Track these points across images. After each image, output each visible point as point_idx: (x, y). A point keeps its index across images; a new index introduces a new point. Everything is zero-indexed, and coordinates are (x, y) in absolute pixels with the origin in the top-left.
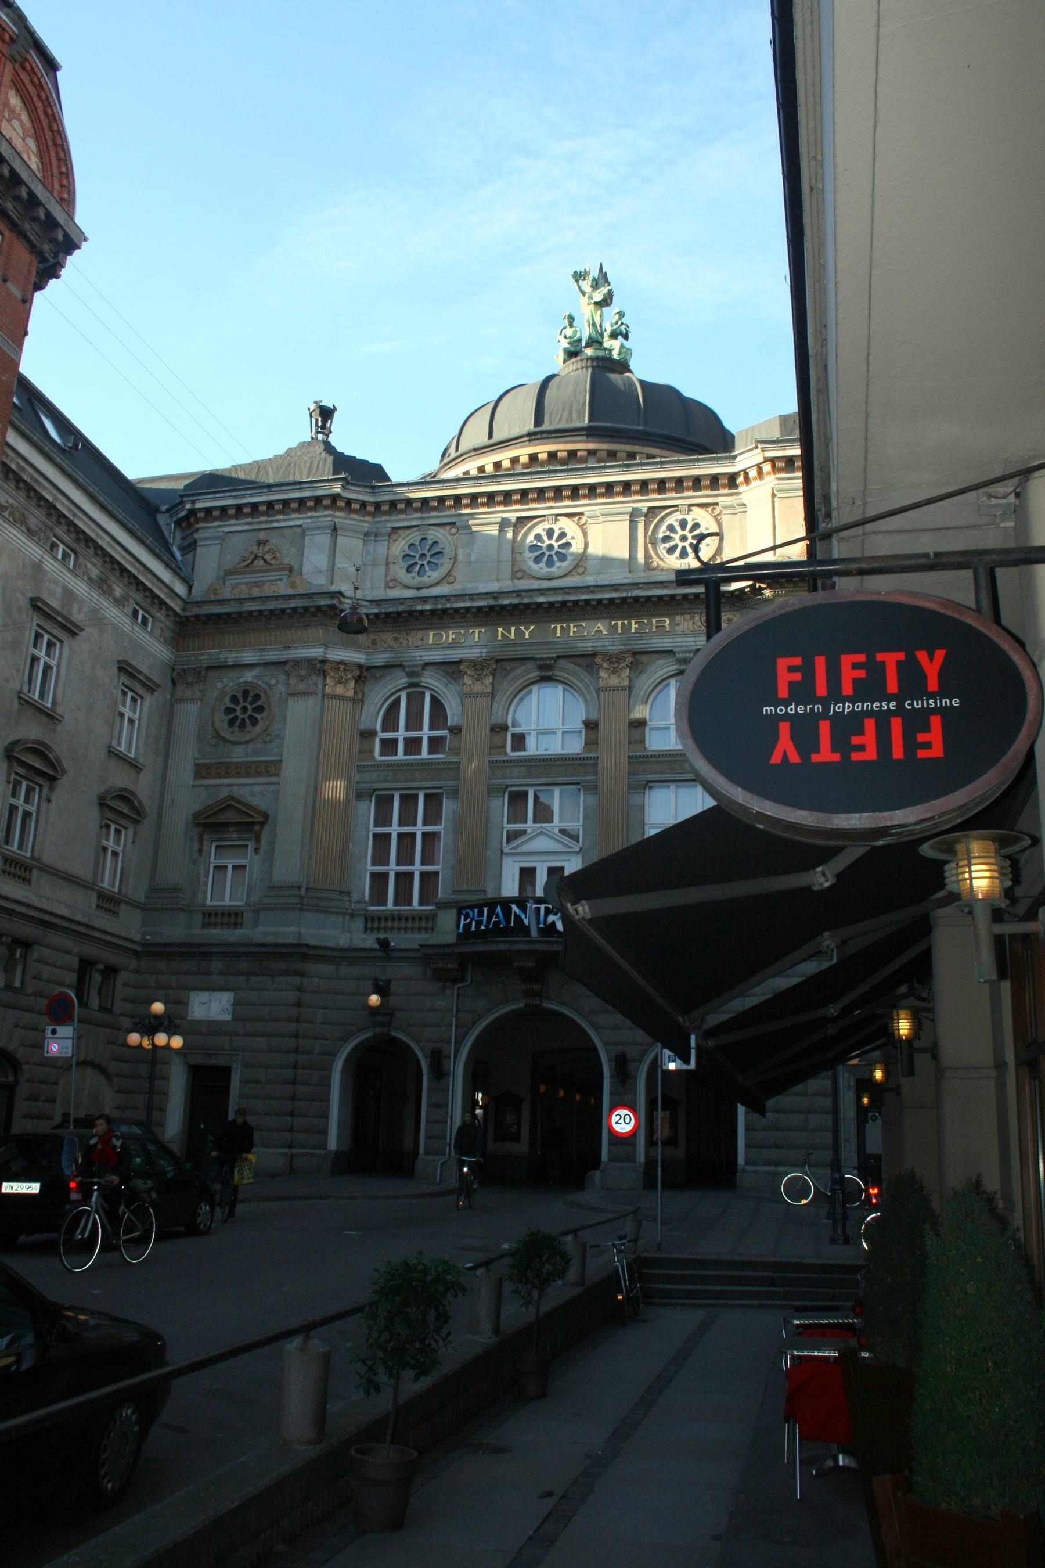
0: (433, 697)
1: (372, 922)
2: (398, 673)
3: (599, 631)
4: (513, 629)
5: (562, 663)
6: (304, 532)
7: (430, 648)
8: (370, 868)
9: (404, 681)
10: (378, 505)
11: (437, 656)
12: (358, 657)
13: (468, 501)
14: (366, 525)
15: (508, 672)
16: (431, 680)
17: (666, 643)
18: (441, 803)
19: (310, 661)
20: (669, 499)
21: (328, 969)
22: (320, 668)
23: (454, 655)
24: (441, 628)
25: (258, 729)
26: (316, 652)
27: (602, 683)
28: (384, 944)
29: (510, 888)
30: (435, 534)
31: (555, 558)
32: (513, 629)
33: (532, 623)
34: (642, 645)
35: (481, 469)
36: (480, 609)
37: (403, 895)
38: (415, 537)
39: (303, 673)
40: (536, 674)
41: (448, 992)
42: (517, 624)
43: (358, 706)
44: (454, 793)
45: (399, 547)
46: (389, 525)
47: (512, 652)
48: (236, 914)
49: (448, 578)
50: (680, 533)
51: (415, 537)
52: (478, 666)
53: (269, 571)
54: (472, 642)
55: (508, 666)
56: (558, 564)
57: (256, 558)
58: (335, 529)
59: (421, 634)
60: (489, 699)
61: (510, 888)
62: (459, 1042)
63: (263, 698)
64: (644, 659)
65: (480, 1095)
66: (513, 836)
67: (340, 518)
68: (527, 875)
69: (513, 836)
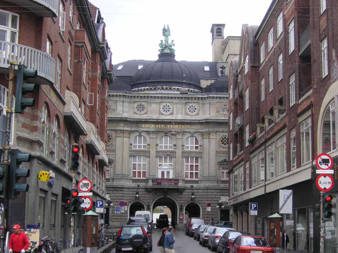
0: (195, 138)
1: (134, 181)
2: (137, 132)
3: (176, 127)
4: (160, 125)
5: (143, 133)
6: (117, 101)
7: (143, 128)
8: (133, 170)
9: (138, 134)
10: (131, 97)
11: (145, 130)
12: (128, 129)
13: (119, 96)
14: (129, 100)
15: (159, 134)
16: (143, 134)
17: (189, 130)
18: (198, 159)
19: (121, 130)
20: (165, 100)
21: (127, 190)
22: (123, 131)
23: (148, 130)
24: (145, 124)
25: (110, 142)
26: (122, 128)
27: (177, 138)
28: (138, 186)
29: (160, 176)
30: (143, 103)
31: (142, 110)
32: (160, 125)
33: (163, 124)
34: (184, 130)
35: (138, 90)
36: (154, 122)
37: (139, 176)
38: (139, 103)
39: (119, 132)
40: (164, 134)
41: (150, 194)
42: (161, 124)
43: (129, 138)
44: (201, 157)
45: (136, 105)
46: (133, 101)
47: (159, 130)
48: (108, 179)
49: (197, 114)
50: (191, 108)
51: (139, 103)
52: (153, 132)
53: (110, 110)
54: (152, 128)
55: (159, 133)
56: (168, 112)
57: (225, 108)
58: (123, 101)
59: (141, 125)
60: (208, 139)
61: (160, 176)
62: (152, 203)
63: (111, 137)
64: (184, 133)
65: (316, 205)
66: (160, 165)
67: (124, 99)
68: (163, 173)
69: (160, 165)
